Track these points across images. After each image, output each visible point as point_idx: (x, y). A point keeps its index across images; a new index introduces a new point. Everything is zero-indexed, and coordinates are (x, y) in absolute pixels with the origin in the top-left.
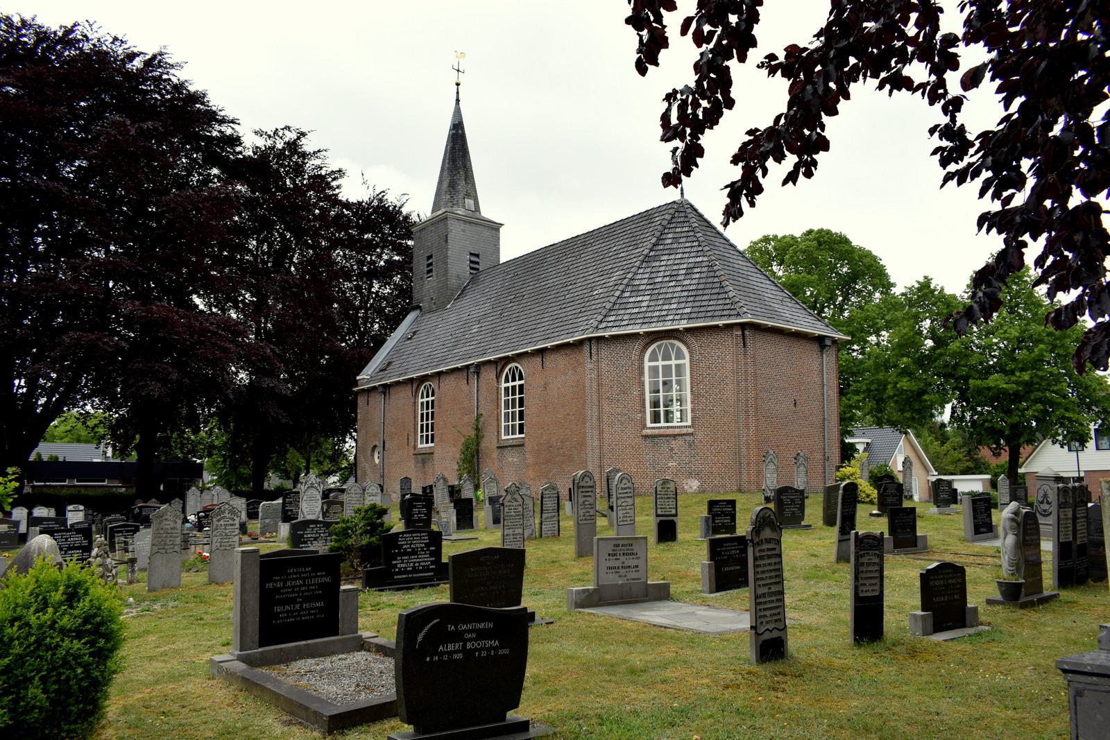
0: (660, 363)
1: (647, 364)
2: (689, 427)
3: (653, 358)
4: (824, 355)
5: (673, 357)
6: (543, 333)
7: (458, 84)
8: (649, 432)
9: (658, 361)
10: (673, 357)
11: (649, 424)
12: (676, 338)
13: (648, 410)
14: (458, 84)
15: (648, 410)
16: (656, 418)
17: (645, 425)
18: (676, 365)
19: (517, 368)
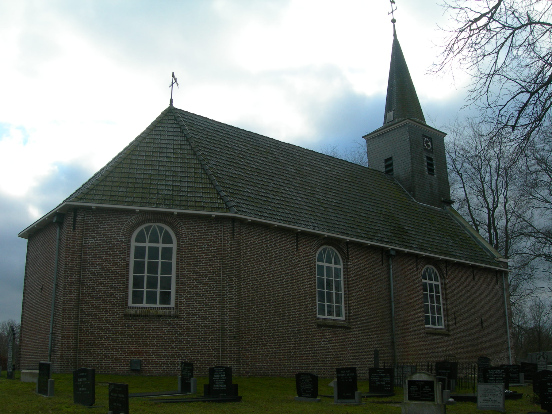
0: (147, 245)
1: (134, 244)
2: (343, 321)
3: (141, 238)
4: (391, 262)
5: (147, 240)
6: (396, 201)
7: (394, 21)
8: (132, 312)
9: (145, 242)
10: (147, 240)
11: (130, 304)
12: (165, 222)
13: (131, 289)
14: (394, 21)
15: (131, 289)
16: (137, 297)
17: (127, 304)
18: (163, 249)
19: (161, 229)
